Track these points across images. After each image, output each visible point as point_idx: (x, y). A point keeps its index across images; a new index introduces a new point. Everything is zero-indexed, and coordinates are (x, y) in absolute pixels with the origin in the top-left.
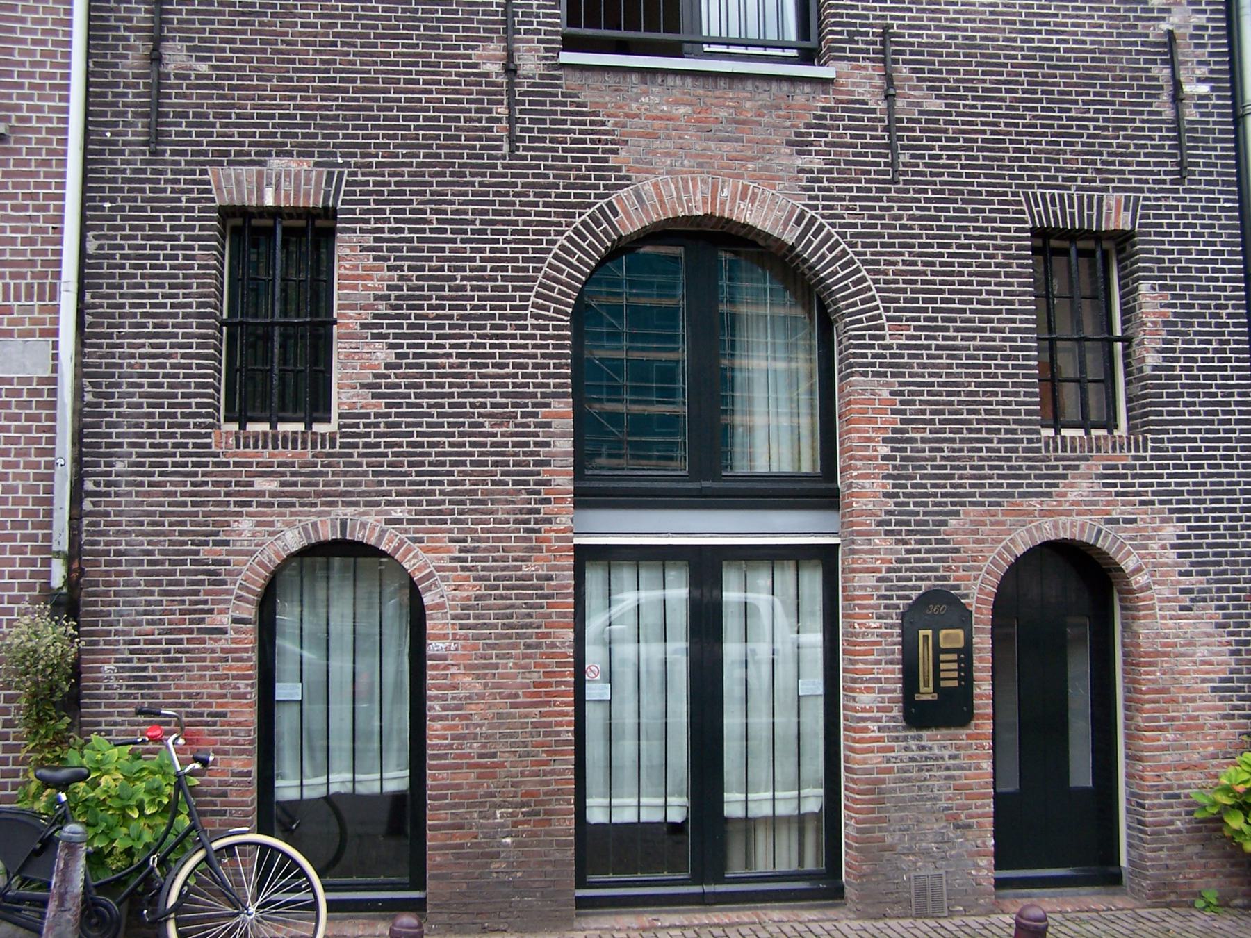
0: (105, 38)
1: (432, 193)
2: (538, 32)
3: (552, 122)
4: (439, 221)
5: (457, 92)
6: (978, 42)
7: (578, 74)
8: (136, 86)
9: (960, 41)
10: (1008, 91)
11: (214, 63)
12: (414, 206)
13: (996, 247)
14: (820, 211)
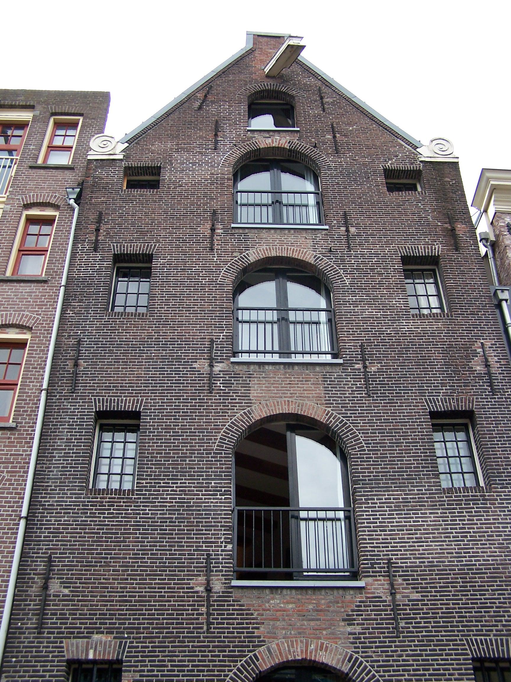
0: (24, 578)
1: (169, 652)
2: (222, 571)
3: (228, 614)
4: (172, 666)
5: (183, 601)
6: (435, 563)
7: (240, 590)
8: (35, 600)
9: (426, 564)
10: (452, 587)
11: (71, 589)
12: (160, 658)
13: (454, 669)
14: (360, 654)
